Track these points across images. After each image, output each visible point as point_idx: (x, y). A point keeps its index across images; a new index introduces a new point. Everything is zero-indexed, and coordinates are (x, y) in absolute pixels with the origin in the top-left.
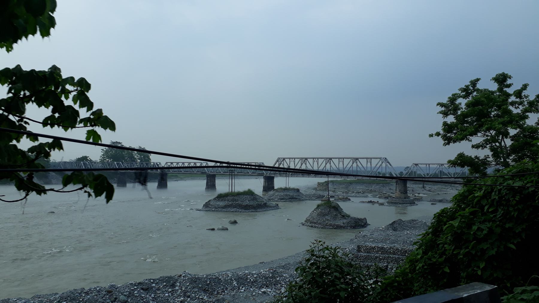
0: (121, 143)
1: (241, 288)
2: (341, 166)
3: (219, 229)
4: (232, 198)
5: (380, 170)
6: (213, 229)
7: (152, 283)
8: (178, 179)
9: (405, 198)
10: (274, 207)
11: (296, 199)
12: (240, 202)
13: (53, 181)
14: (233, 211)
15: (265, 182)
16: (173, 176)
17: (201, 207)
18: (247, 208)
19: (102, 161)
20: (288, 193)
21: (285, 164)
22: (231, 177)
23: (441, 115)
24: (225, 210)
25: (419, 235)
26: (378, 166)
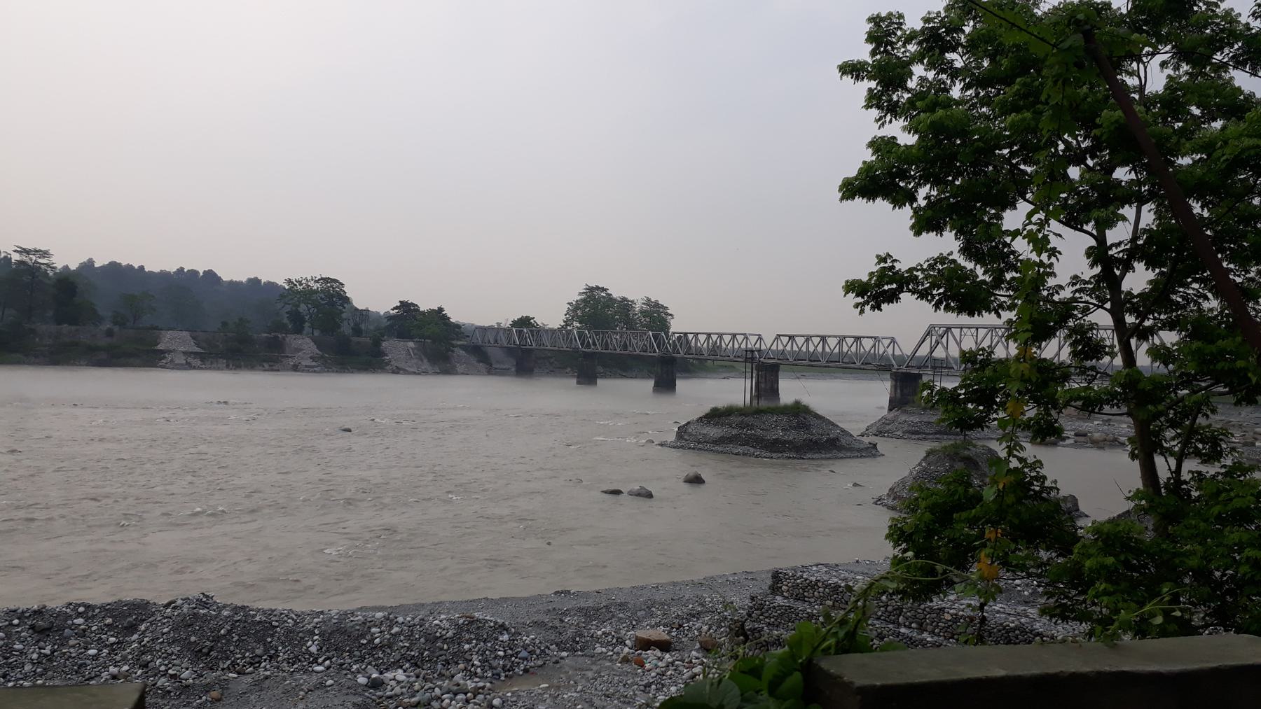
1: (320, 660)
3: (631, 493)
4: (740, 419)
7: (79, 615)
8: (732, 374)
10: (859, 450)
13: (460, 368)
15: (895, 387)
16: (722, 366)
17: (671, 437)
18: (774, 447)
21: (952, 342)
23: (875, 113)
24: (720, 449)
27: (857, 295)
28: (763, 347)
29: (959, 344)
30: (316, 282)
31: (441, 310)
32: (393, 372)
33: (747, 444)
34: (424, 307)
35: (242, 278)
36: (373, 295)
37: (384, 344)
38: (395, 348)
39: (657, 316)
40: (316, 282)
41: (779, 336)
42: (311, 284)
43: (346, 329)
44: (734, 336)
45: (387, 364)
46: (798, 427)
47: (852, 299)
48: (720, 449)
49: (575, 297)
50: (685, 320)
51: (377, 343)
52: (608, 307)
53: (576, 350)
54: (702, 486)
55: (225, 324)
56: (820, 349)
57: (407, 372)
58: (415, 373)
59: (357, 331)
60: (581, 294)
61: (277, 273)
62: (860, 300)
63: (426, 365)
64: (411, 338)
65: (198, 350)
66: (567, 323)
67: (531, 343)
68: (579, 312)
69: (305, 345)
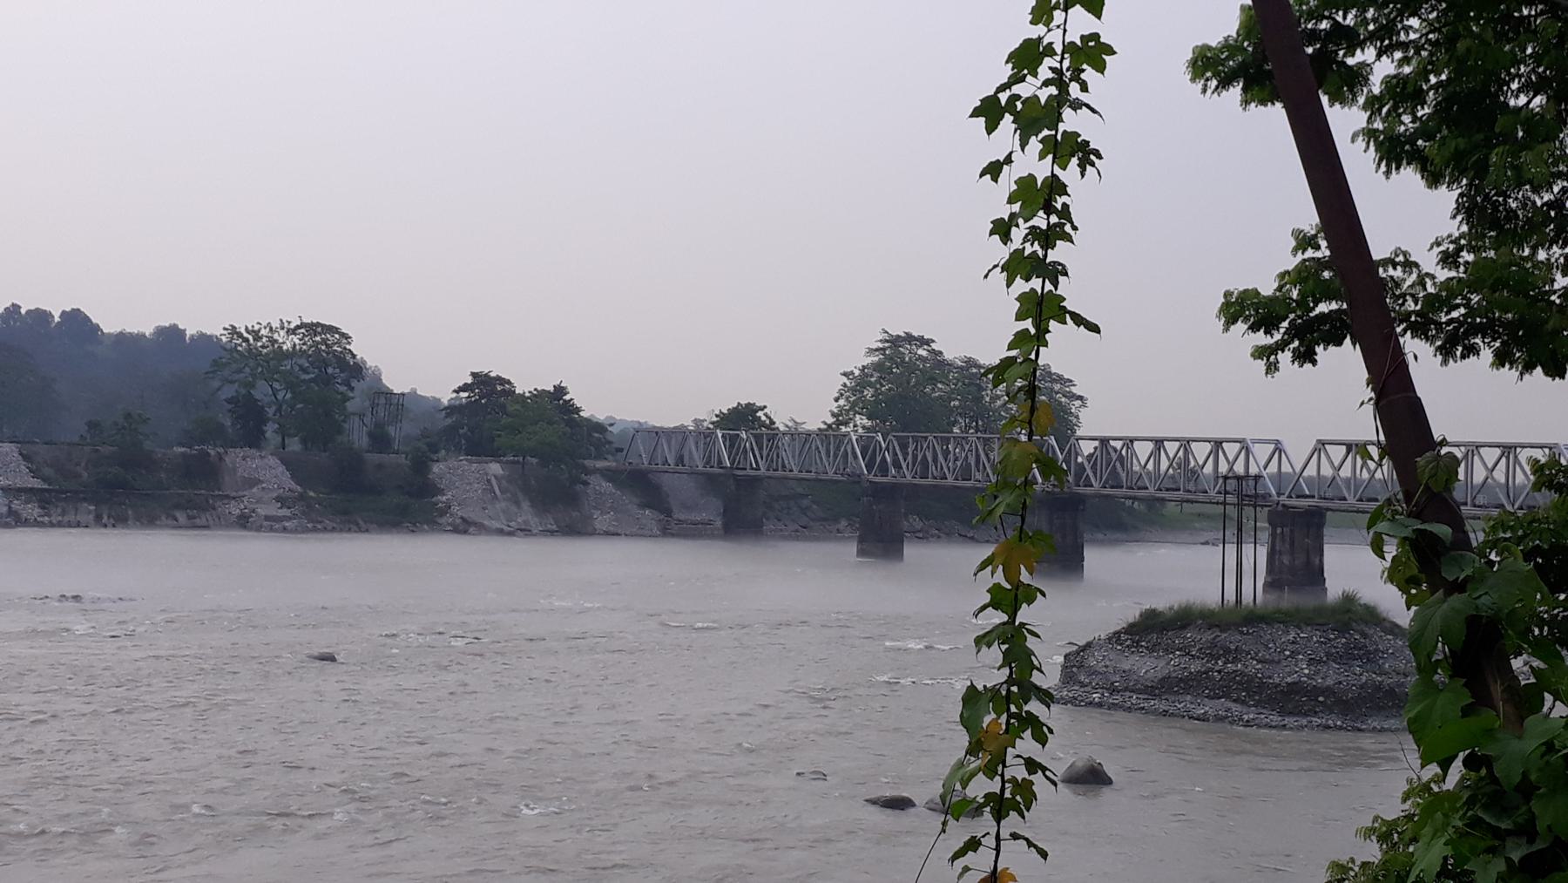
0: (928, 342)
4: (1208, 636)
6: (899, 804)
12: (1253, 667)
13: (601, 521)
14: (1165, 713)
18: (1293, 702)
19: (830, 436)
22: (1231, 533)
25: (907, 844)
27: (1254, 328)
28: (1286, 468)
30: (293, 332)
31: (560, 391)
32: (457, 530)
33: (1226, 696)
34: (523, 387)
35: (144, 324)
36: (418, 361)
37: (436, 468)
38: (458, 476)
40: (293, 332)
41: (1322, 443)
42: (280, 336)
43: (358, 436)
44: (1218, 444)
45: (443, 513)
46: (1345, 657)
47: (1244, 339)
48: (1163, 706)
49: (858, 360)
51: (421, 465)
52: (933, 380)
53: (856, 478)
54: (1106, 790)
55: (93, 426)
56: (1150, 466)
57: (482, 529)
58: (501, 532)
59: (380, 441)
60: (871, 351)
61: (207, 315)
62: (1261, 339)
63: (526, 514)
64: (495, 455)
65: (37, 483)
66: (841, 418)
67: (757, 465)
68: (868, 393)
69: (263, 470)
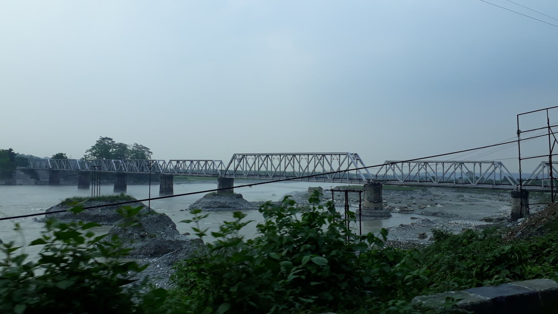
2: (423, 171)
5: (492, 177)
9: (376, 209)
11: (229, 207)
13: (18, 181)
19: (83, 161)
20: (219, 200)
26: (490, 171)
29: (330, 165)
31: (11, 150)
38: (19, 172)
39: (140, 154)
44: (206, 161)
50: (162, 154)
56: (212, 168)
